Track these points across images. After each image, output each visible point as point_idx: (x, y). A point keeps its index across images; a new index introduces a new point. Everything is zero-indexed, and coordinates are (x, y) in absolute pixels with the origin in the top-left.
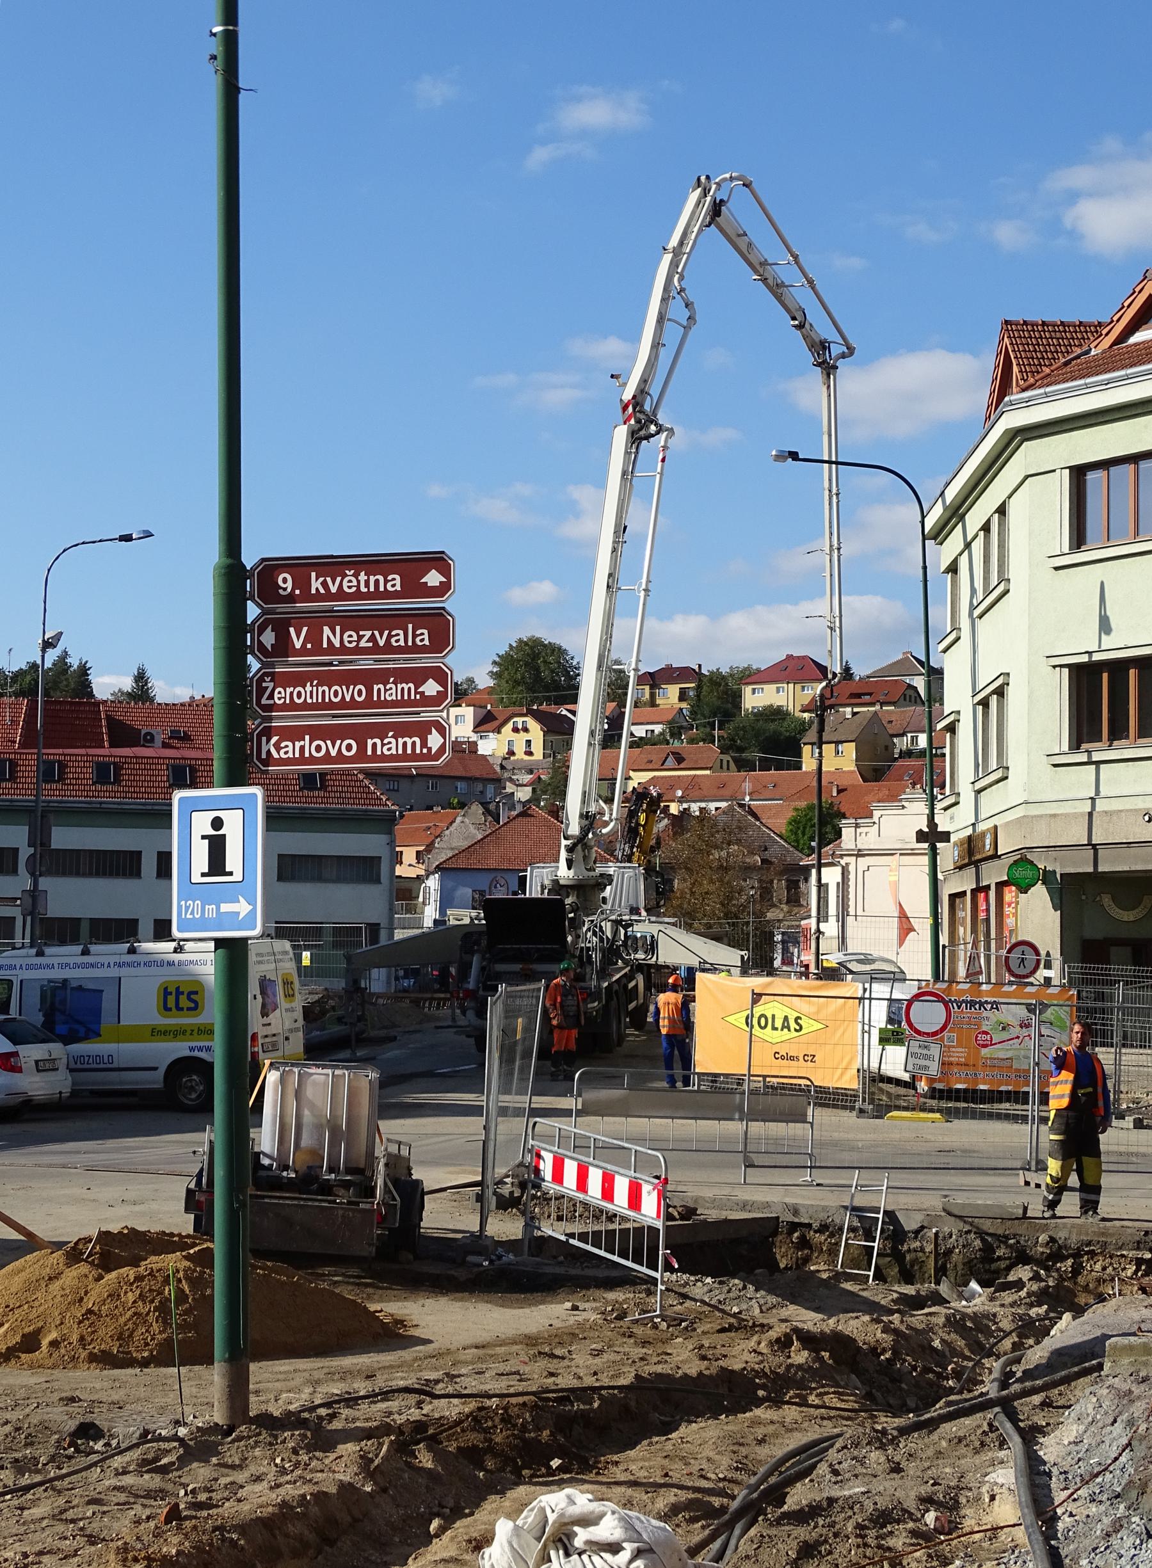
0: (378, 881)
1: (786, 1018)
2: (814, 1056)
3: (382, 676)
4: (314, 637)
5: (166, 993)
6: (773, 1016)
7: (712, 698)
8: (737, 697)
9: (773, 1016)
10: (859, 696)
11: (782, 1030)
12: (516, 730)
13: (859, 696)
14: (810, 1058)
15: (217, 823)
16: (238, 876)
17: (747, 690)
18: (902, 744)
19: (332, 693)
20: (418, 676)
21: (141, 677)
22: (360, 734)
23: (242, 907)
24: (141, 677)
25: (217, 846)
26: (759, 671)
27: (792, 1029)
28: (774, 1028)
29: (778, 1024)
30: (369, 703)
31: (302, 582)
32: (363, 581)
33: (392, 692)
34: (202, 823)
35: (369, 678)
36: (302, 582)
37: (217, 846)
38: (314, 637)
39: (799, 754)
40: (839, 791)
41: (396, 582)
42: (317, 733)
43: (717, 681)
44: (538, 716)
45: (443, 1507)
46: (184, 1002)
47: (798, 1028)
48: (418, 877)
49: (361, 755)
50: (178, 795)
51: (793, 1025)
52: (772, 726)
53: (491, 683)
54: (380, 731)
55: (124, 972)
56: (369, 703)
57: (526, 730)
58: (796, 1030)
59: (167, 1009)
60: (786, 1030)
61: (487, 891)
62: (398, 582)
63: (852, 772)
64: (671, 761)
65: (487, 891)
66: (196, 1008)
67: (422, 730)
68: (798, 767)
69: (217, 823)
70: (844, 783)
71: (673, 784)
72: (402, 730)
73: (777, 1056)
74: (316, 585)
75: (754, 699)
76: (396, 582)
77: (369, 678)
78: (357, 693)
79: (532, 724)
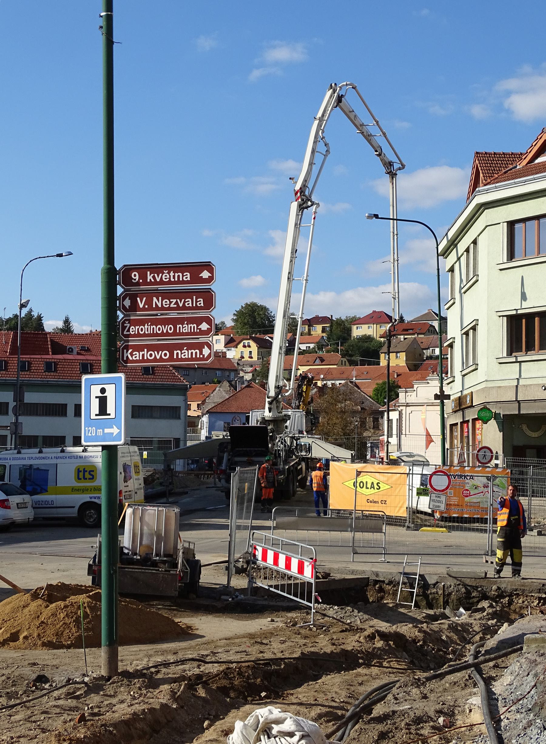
0: (179, 418)
1: (373, 483)
2: (386, 501)
3: (181, 321)
4: (149, 302)
5: (79, 471)
6: (367, 482)
7: (337, 331)
8: (349, 331)
9: (367, 482)
10: (407, 330)
11: (371, 489)
12: (244, 346)
13: (407, 330)
14: (384, 502)
15: (103, 391)
16: (113, 416)
17: (354, 327)
18: (427, 353)
19: (158, 329)
20: (198, 321)
21: (67, 321)
22: (171, 348)
23: (115, 431)
24: (67, 321)
25: (103, 402)
26: (360, 318)
27: (375, 488)
28: (367, 488)
29: (369, 486)
30: (175, 333)
31: (143, 276)
32: (172, 276)
33: (186, 328)
34: (96, 391)
35: (175, 322)
36: (143, 276)
37: (103, 402)
38: (149, 302)
39: (379, 358)
40: (398, 376)
41: (187, 276)
42: (150, 348)
43: (340, 323)
44: (255, 340)
45: (210, 715)
46: (87, 475)
47: (378, 488)
48: (198, 416)
49: (171, 358)
50: (84, 377)
51: (376, 486)
52: (366, 345)
53: (233, 324)
54: (180, 347)
55: (59, 461)
56: (175, 333)
57: (249, 346)
58: (377, 489)
59: (79, 479)
60: (372, 489)
61: (231, 423)
62: (189, 276)
63: (404, 366)
64: (318, 361)
65: (231, 423)
66: (93, 478)
67: (200, 346)
68: (378, 364)
69: (103, 391)
70: (400, 371)
71: (319, 372)
72: (190, 346)
73: (368, 501)
74: (150, 277)
75: (357, 332)
76: (187, 276)
77: (175, 322)
78: (169, 329)
79: (252, 343)
